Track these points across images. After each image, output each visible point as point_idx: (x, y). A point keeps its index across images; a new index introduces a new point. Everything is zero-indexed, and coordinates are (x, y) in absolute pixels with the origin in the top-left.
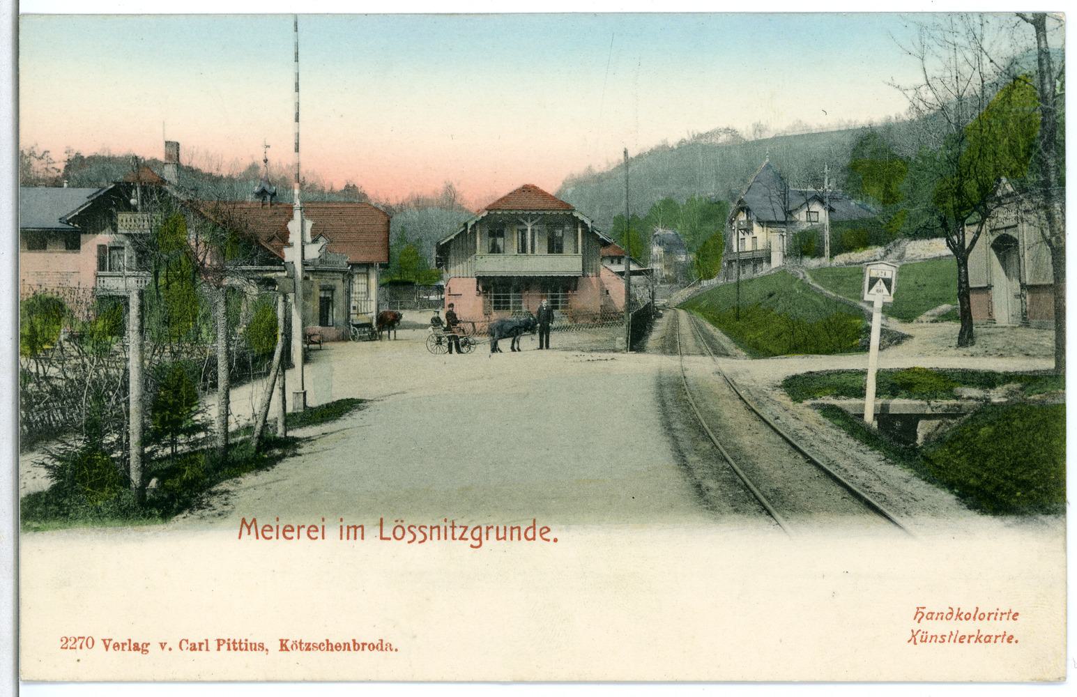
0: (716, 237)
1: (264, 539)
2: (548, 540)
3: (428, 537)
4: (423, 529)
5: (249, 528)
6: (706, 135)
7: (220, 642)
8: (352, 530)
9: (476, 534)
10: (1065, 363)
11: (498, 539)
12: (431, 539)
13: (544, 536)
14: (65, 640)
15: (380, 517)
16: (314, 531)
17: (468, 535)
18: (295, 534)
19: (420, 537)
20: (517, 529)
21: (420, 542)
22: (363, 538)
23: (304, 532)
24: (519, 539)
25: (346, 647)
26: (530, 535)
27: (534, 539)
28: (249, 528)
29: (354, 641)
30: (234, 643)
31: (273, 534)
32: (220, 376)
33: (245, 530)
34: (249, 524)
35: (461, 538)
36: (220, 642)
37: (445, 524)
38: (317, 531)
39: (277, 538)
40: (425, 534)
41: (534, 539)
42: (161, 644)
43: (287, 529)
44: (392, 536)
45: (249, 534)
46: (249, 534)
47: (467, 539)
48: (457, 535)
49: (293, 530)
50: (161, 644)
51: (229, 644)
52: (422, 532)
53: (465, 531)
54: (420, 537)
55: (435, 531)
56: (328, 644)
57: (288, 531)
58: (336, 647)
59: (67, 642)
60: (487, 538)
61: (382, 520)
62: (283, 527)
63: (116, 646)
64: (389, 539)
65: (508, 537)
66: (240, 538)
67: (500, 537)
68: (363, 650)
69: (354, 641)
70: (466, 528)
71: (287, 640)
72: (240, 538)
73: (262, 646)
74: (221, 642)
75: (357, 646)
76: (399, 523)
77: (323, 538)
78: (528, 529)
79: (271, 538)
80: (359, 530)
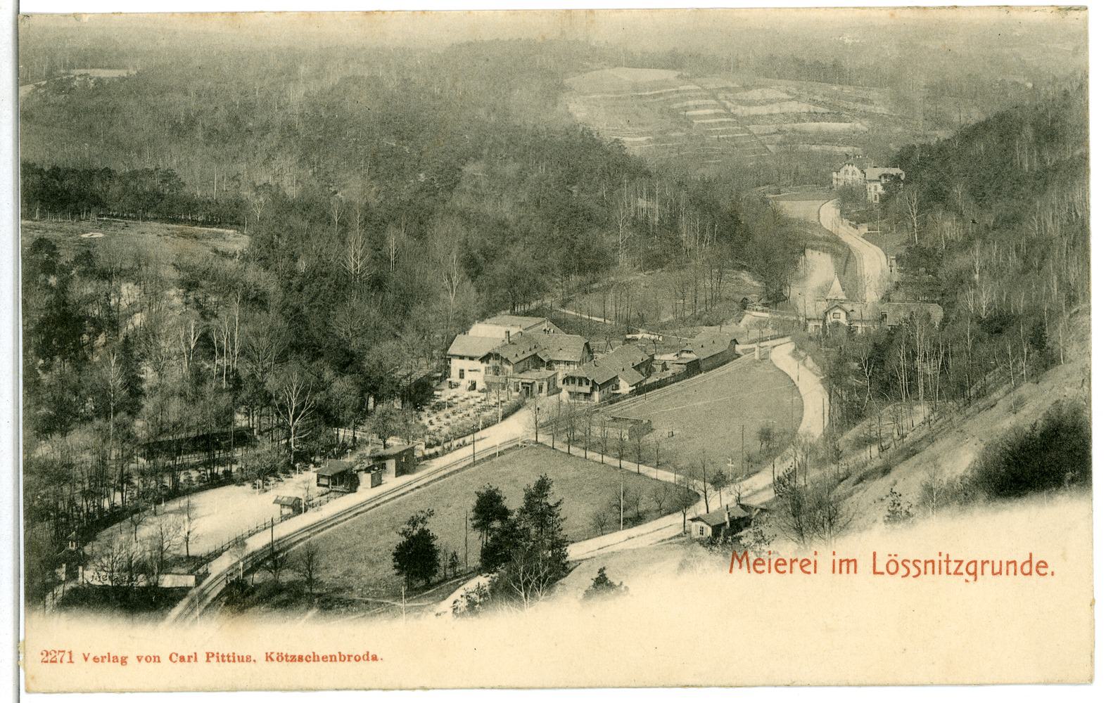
1: (755, 573)
2: (809, 573)
4: (917, 563)
5: (740, 561)
7: (209, 656)
8: (844, 565)
9: (971, 569)
11: (994, 574)
12: (925, 573)
13: (805, 569)
14: (45, 653)
16: (1043, 567)
17: (962, 569)
18: (787, 568)
19: (914, 571)
20: (1013, 564)
21: (914, 577)
22: (855, 572)
23: (796, 566)
25: (332, 658)
26: (1027, 569)
27: (1030, 573)
28: (740, 561)
29: (340, 653)
30: (287, 656)
31: (766, 568)
33: (736, 564)
34: (740, 558)
35: (956, 573)
36: (209, 656)
38: (764, 564)
39: (769, 572)
40: (919, 569)
41: (1030, 573)
42: (138, 657)
43: (780, 562)
44: (885, 571)
45: (741, 567)
46: (741, 567)
47: (962, 574)
48: (952, 570)
49: (785, 564)
50: (138, 657)
51: (218, 657)
52: (916, 566)
53: (959, 565)
54: (914, 571)
55: (930, 566)
56: (314, 656)
57: (806, 565)
58: (323, 658)
59: (47, 655)
60: (983, 574)
62: (776, 559)
63: (96, 659)
64: (882, 573)
65: (1004, 572)
66: (731, 571)
68: (349, 660)
69: (340, 653)
70: (961, 562)
71: (272, 653)
72: (731, 571)
73: (249, 659)
74: (210, 655)
75: (315, 658)
76: (893, 557)
77: (791, 572)
78: (1024, 564)
79: (785, 572)
80: (852, 565)
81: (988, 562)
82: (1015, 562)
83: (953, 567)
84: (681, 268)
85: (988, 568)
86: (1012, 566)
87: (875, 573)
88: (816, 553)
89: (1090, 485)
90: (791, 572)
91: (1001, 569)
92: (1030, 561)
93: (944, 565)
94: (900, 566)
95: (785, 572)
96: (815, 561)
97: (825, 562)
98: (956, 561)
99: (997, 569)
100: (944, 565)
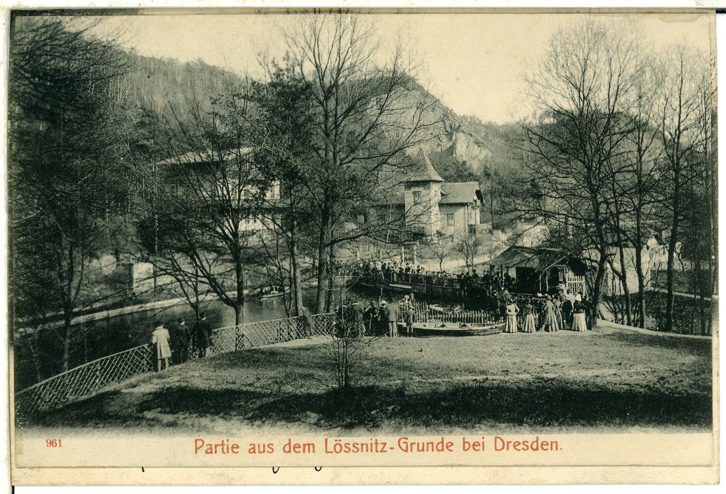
0: (224, 82)
2: (519, 450)
3: (360, 450)
6: (718, 324)
8: (307, 447)
10: (10, 74)
15: (221, 440)
22: (314, 452)
24: (433, 450)
26: (535, 446)
27: (443, 450)
32: (285, 346)
35: (382, 451)
37: (483, 440)
44: (333, 450)
49: (479, 445)
55: (365, 447)
61: (326, 440)
64: (332, 452)
67: (555, 443)
76: (338, 442)
77: (483, 450)
78: (438, 444)
79: (299, 452)
80: (311, 447)
81: (414, 443)
82: (432, 443)
83: (380, 447)
84: (438, 388)
85: (415, 447)
86: (430, 445)
87: (327, 452)
88: (483, 438)
89: (712, 428)
90: (483, 450)
91: (423, 447)
92: (289, 444)
93: (374, 446)
94: (530, 447)
95: (479, 450)
96: (483, 443)
97: (244, 447)
98: (382, 443)
99: (421, 448)
100: (374, 446)
